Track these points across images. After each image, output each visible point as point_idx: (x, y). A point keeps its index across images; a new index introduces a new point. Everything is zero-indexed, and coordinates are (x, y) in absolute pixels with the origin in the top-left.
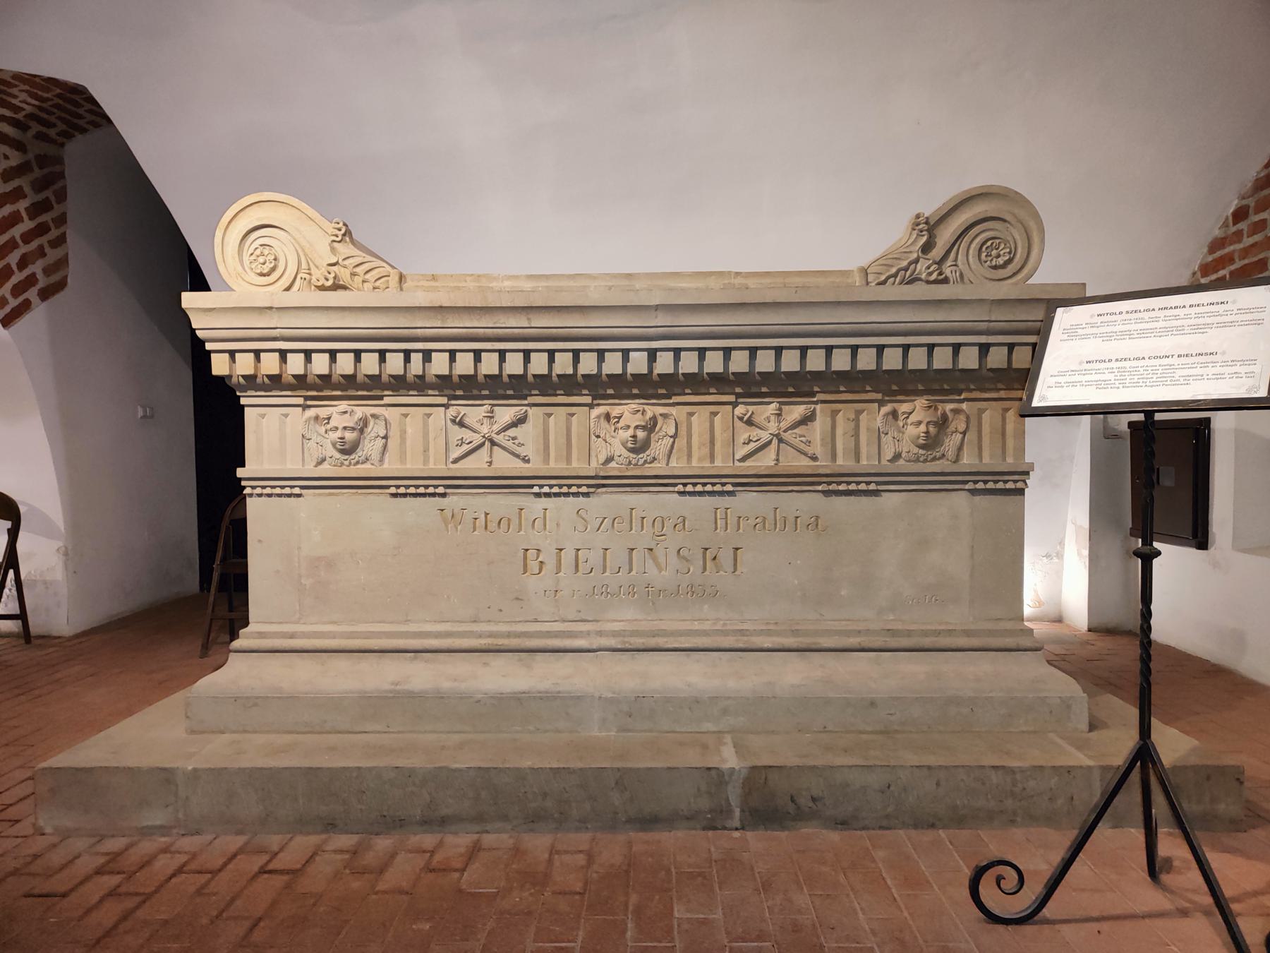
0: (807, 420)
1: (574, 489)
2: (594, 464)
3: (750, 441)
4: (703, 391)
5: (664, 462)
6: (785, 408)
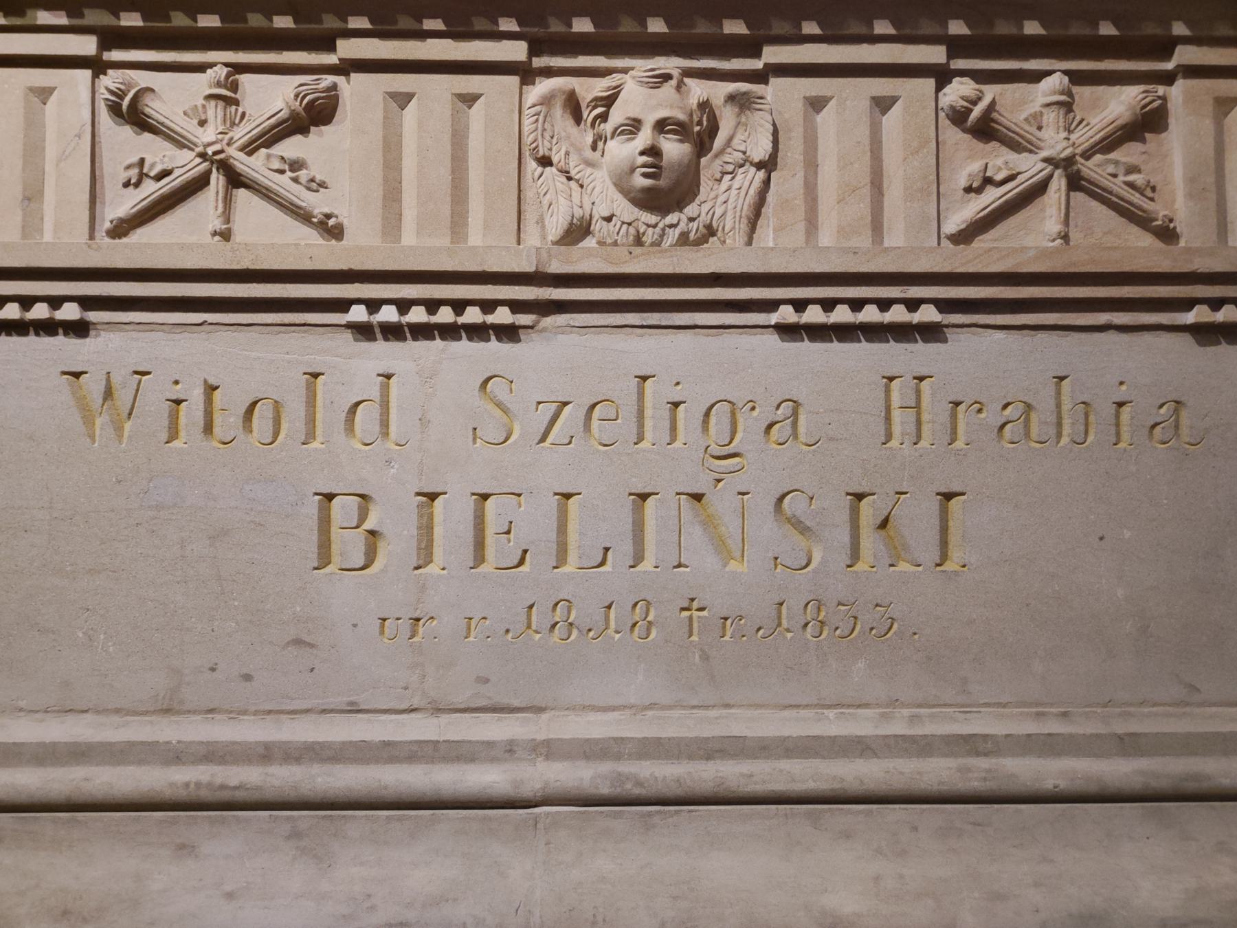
0: (1149, 123)
1: (472, 315)
2: (532, 238)
3: (988, 181)
4: (856, 28)
5: (740, 239)
6: (1084, 93)
